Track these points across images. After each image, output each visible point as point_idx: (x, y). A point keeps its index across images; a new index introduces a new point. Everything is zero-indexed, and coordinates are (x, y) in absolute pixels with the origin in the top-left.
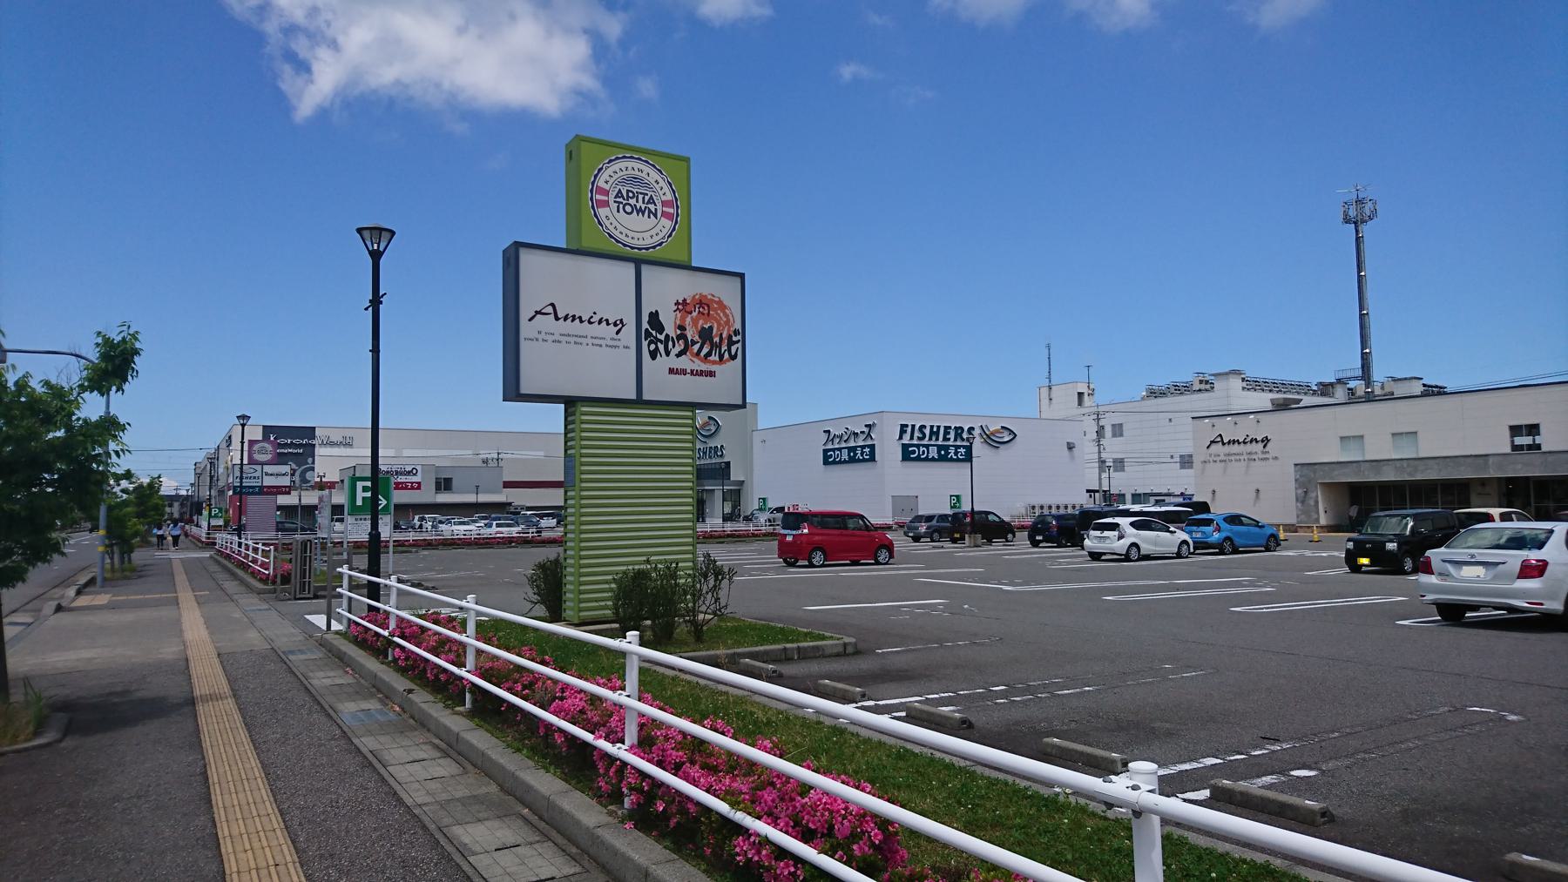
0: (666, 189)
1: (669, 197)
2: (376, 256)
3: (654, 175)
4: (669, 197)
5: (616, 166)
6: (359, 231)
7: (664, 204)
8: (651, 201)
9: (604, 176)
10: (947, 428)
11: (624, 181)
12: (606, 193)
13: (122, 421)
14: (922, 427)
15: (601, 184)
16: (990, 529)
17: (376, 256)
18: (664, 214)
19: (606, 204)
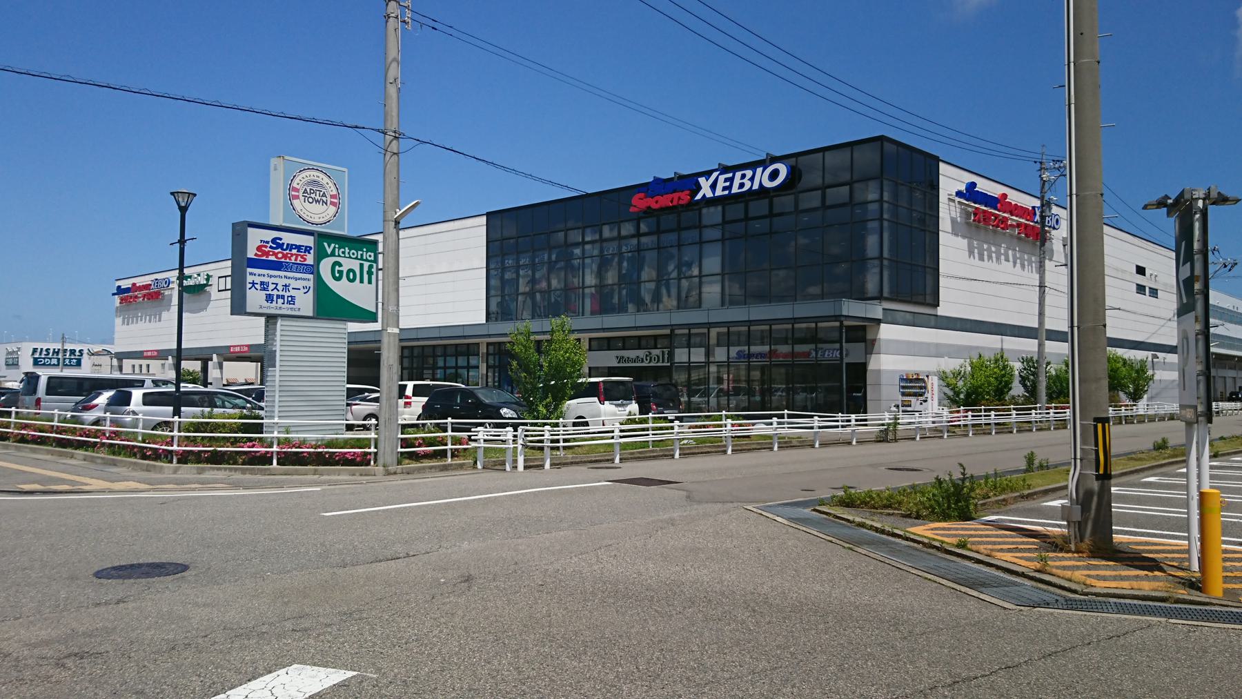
0: (333, 188)
1: (335, 192)
2: (183, 210)
3: (326, 180)
4: (335, 192)
5: (304, 174)
6: (172, 194)
7: (332, 197)
8: (324, 195)
9: (297, 181)
10: (1225, 569)
11: (309, 183)
12: (297, 190)
13: (1160, 441)
14: (47, 350)
15: (295, 185)
16: (265, 459)
17: (183, 210)
18: (332, 203)
19: (297, 197)
